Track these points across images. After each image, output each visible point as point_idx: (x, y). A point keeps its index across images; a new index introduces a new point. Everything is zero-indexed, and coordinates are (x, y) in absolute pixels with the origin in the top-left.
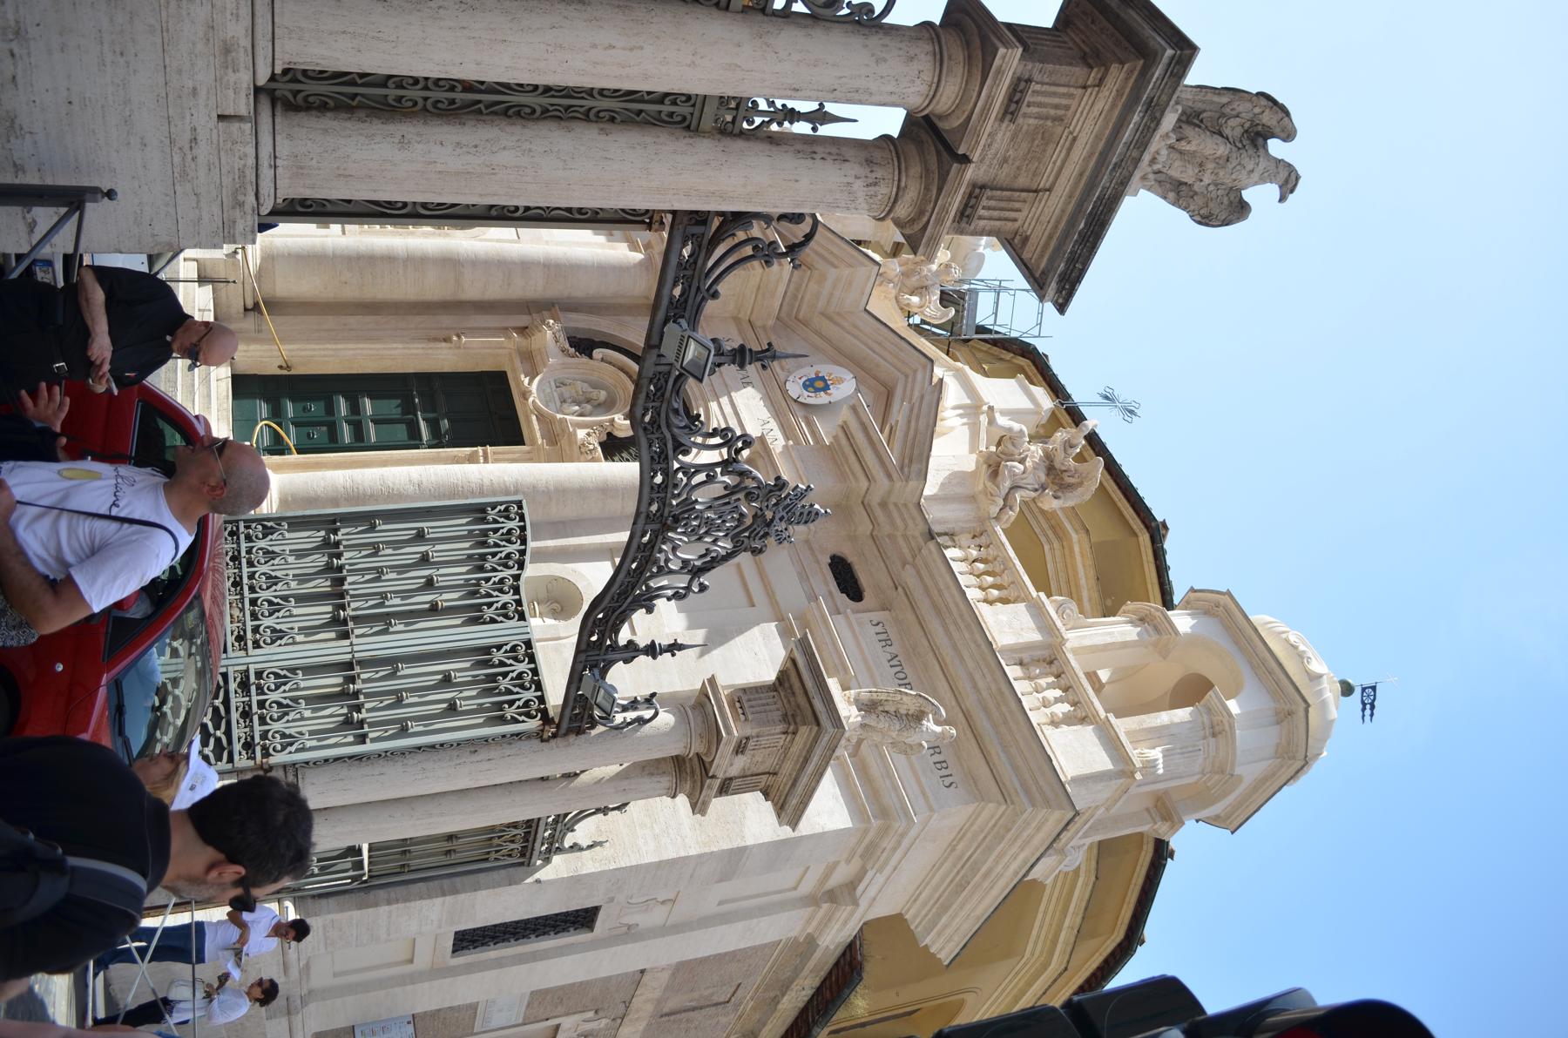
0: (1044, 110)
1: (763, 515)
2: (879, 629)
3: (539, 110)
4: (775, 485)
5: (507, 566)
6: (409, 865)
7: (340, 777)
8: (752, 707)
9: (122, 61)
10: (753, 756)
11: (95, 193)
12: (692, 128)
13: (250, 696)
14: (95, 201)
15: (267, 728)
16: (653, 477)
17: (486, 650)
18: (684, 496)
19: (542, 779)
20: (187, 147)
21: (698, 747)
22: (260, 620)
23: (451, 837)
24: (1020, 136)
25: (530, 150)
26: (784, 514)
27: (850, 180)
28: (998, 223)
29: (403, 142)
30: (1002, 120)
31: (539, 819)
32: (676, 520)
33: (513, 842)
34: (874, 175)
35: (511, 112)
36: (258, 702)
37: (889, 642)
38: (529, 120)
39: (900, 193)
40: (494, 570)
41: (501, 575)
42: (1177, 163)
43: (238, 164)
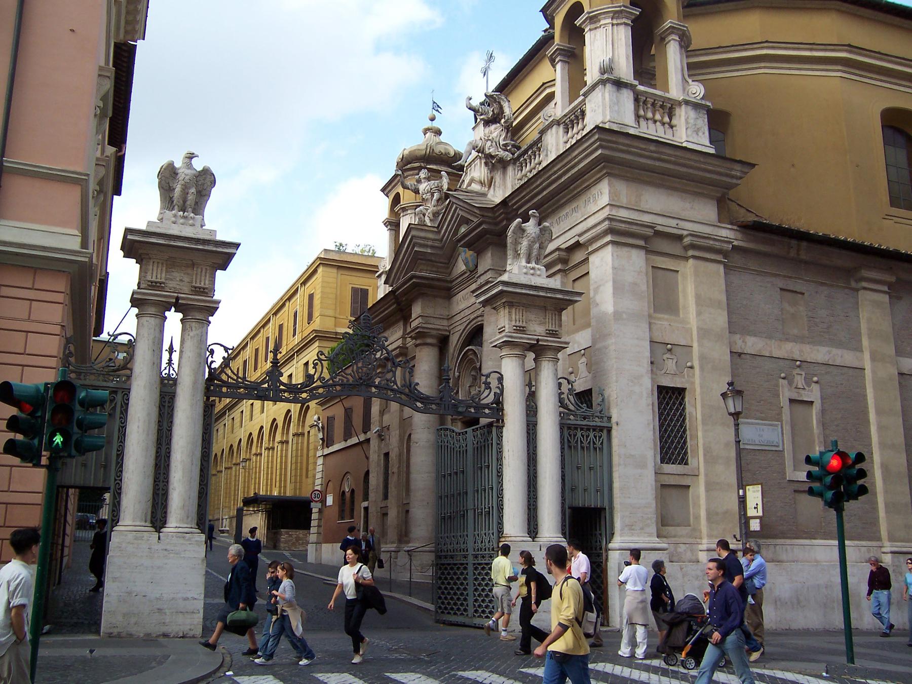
27: (189, 337)
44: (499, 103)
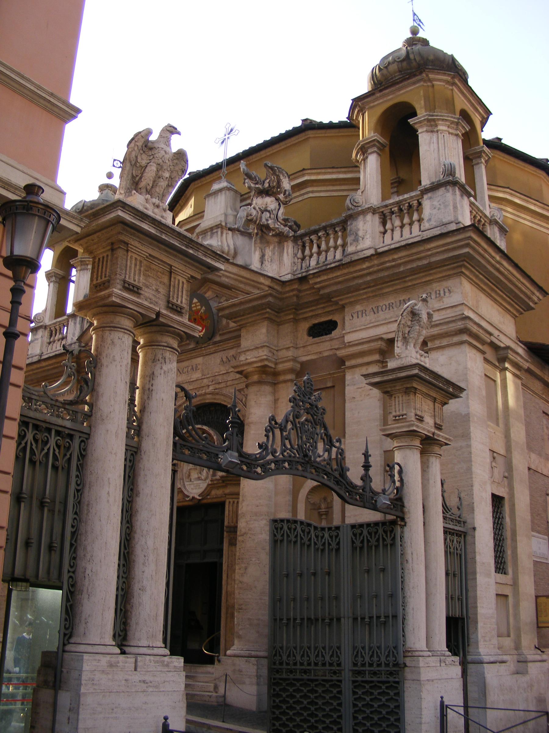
0: (137, 272)
1: (307, 409)
2: (355, 316)
3: (128, 525)
4: (293, 403)
5: (309, 533)
6: (458, 596)
7: (412, 629)
8: (399, 410)
9: (115, 710)
10: (425, 411)
11: (442, 703)
12: (136, 450)
13: (366, 670)
14: (168, 725)
15: (327, 663)
16: (286, 468)
17: (354, 549)
18: (295, 451)
19: (424, 525)
20: (146, 685)
21: (417, 443)
22: (297, 662)
23: (447, 574)
24: (147, 283)
25: (147, 531)
26: (307, 397)
27: (163, 371)
28: (184, 292)
29: (143, 589)
30: (140, 294)
31: (444, 527)
32: (306, 456)
33: (453, 541)
34: (161, 359)
35: (128, 538)
36: (385, 667)
37: (364, 311)
38: (132, 529)
39: (170, 346)
40: (310, 540)
41: (313, 536)
42: (157, 190)
43: (152, 663)
44: (278, 176)
